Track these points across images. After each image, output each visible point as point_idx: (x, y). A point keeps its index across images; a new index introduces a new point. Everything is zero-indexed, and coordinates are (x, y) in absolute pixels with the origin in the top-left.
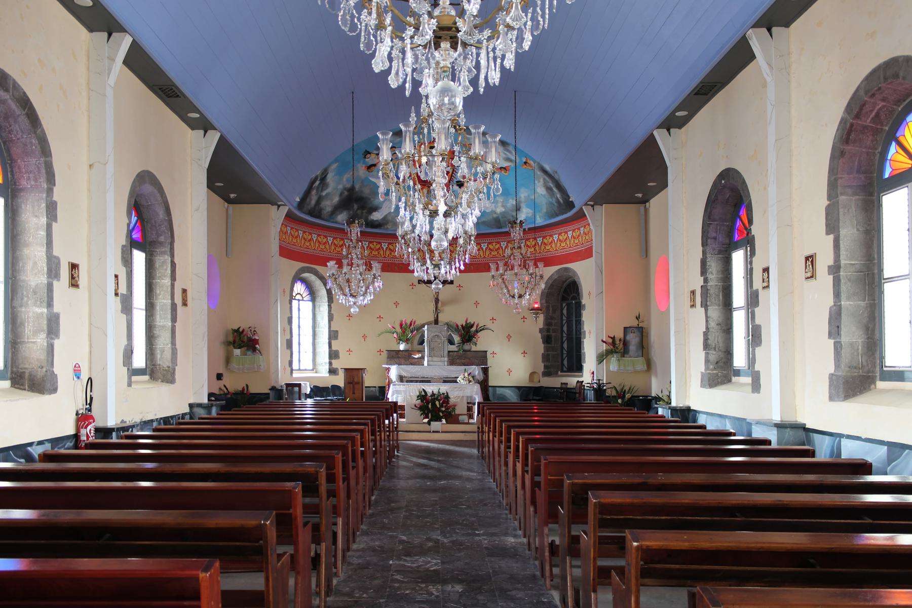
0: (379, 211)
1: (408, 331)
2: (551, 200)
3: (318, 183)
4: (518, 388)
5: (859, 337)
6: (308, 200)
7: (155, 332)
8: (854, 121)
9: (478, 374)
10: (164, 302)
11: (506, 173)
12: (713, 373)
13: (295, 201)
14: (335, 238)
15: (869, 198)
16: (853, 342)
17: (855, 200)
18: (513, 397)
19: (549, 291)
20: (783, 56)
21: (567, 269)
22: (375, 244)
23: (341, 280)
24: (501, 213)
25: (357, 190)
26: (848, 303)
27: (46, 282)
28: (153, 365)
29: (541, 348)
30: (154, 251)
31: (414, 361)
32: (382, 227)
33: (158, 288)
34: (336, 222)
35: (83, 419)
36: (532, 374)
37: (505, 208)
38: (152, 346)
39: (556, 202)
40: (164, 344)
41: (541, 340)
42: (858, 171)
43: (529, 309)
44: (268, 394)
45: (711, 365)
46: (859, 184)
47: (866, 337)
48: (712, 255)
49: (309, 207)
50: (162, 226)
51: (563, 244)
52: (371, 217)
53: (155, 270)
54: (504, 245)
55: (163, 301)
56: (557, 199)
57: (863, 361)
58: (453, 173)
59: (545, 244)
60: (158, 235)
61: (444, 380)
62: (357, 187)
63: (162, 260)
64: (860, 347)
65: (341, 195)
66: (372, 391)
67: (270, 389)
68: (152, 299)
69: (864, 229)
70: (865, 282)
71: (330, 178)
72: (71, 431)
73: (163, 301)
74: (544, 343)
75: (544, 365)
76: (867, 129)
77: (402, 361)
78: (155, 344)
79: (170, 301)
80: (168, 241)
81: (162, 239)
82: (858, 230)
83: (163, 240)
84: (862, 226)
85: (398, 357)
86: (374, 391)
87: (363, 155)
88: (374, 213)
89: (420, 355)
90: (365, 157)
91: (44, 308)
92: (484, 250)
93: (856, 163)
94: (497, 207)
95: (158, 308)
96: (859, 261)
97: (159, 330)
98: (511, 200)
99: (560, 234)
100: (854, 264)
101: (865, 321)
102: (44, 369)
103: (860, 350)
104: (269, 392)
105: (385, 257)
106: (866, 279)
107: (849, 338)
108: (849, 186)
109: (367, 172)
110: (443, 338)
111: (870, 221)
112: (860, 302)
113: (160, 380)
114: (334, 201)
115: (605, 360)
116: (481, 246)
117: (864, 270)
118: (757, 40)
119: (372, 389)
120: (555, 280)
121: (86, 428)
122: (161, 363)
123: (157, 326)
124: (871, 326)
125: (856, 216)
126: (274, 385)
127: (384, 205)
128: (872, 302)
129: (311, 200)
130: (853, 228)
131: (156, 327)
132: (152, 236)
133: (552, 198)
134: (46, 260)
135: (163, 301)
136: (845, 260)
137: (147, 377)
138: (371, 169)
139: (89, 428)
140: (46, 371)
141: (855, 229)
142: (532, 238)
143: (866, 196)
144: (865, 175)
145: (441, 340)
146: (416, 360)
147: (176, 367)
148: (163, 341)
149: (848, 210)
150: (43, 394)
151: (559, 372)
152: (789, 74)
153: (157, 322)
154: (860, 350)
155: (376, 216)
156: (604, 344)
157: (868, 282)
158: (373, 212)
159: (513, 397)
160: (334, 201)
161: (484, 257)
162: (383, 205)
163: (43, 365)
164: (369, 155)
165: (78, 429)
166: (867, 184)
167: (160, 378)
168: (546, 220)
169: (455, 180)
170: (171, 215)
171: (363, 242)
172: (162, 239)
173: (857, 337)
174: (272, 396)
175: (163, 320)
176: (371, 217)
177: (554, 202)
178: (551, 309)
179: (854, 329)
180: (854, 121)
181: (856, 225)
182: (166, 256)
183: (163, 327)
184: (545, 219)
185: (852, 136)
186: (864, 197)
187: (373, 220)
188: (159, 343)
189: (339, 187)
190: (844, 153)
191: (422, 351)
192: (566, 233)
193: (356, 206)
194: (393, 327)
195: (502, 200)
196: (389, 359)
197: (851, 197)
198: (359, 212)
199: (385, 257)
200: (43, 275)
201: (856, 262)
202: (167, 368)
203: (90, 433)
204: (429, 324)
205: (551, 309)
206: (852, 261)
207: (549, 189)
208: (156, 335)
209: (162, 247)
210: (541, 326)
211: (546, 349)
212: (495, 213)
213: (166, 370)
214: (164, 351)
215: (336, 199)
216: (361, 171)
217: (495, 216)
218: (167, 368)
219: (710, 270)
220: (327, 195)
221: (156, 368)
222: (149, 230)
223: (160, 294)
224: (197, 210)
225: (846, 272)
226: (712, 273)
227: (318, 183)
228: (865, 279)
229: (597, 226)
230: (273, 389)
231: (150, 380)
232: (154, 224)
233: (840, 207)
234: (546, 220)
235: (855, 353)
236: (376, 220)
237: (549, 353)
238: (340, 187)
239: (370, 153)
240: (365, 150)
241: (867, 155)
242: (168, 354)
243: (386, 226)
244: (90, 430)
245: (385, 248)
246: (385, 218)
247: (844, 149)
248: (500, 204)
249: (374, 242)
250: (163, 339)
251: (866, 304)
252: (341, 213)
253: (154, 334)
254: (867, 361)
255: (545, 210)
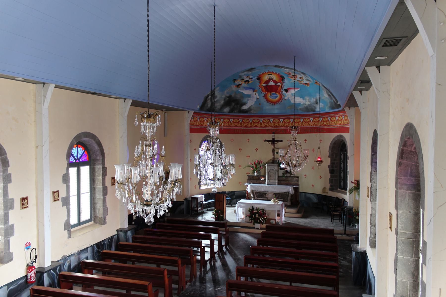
0: (246, 105)
1: (258, 165)
2: (331, 100)
3: (210, 97)
4: (317, 195)
5: (408, 279)
6: (206, 105)
7: (96, 201)
8: (403, 148)
9: (291, 191)
10: (99, 187)
11: (308, 86)
12: (373, 240)
13: (197, 108)
14: (224, 119)
15: (418, 192)
16: (404, 281)
17: (408, 193)
18: (315, 200)
19: (333, 146)
20: (386, 83)
21: (341, 136)
22: (246, 120)
23: (161, 189)
24: (308, 105)
25: (233, 96)
26: (402, 257)
27: (3, 213)
28: (95, 216)
29: (328, 176)
30: (95, 163)
31: (261, 181)
32: (249, 113)
33: (97, 180)
34: (223, 112)
35: (30, 268)
36: (324, 189)
37: (310, 102)
38: (95, 207)
39: (334, 102)
40: (100, 207)
41: (329, 172)
42: (411, 176)
43: (315, 161)
44: (183, 202)
45: (372, 235)
46: (411, 184)
47: (412, 280)
48: (375, 172)
49: (207, 108)
50: (98, 152)
51: (340, 122)
52: (242, 108)
53: (95, 173)
54: (312, 120)
55: (99, 187)
56: (334, 100)
57: (411, 294)
58: (282, 85)
59: (332, 121)
60: (96, 156)
61: (274, 193)
62: (233, 95)
63: (99, 168)
64: (408, 285)
65: (225, 100)
66: (244, 193)
67: (184, 200)
68: (94, 186)
69: (414, 212)
70: (414, 246)
71: (217, 93)
72: (24, 274)
73: (99, 187)
74: (330, 173)
75: (330, 185)
76: (413, 153)
77: (255, 181)
78: (95, 206)
79: (102, 187)
80: (101, 159)
81: (98, 158)
82: (410, 212)
83: (98, 158)
84: (413, 210)
85: (253, 179)
86: (245, 193)
87: (233, 81)
88: (243, 106)
89: (264, 179)
90: (234, 82)
91: (2, 225)
92: (302, 122)
93: (409, 171)
94: (306, 101)
95: (97, 190)
96: (409, 232)
97: (98, 200)
98: (313, 99)
99: (339, 116)
100: (407, 233)
101: (412, 270)
102: (3, 253)
103: (408, 287)
104: (184, 201)
105: (251, 126)
106: (414, 243)
107: (401, 279)
108: (405, 184)
109: (237, 88)
110: (275, 171)
111: (418, 208)
112: (409, 258)
113: (98, 223)
114: (221, 103)
115: (353, 192)
116: (300, 120)
117: (412, 238)
118: (372, 72)
119: (243, 192)
120: (336, 141)
121: (30, 273)
122: (98, 215)
123: (96, 198)
124: (416, 274)
125: (409, 203)
126: (187, 197)
127: (248, 102)
128: (417, 259)
129: (208, 105)
130: (407, 211)
131: (96, 199)
132: (93, 157)
133: (331, 100)
134: (3, 203)
135: (99, 186)
136: (401, 230)
137: (92, 222)
138: (239, 86)
139: (31, 273)
140: (4, 254)
141: (408, 211)
142: (326, 117)
143: (416, 191)
144: (415, 178)
145: (274, 171)
146: (262, 181)
147: (107, 216)
148: (99, 206)
149: (404, 199)
150: (3, 264)
151: (338, 189)
152: (389, 95)
153: (96, 196)
154: (408, 287)
155: (245, 107)
156: (353, 184)
157: (415, 246)
158: (243, 106)
159: (315, 200)
160: (221, 103)
161: (302, 126)
162: (247, 102)
163: (3, 251)
164: (236, 81)
165: (27, 273)
166: (416, 184)
167: (98, 222)
168: (330, 110)
169: (283, 89)
170: (102, 146)
171: (240, 119)
172: (98, 158)
173: (407, 279)
174: (185, 203)
175: (99, 196)
176: (242, 108)
177: (332, 101)
178: (334, 155)
179: (405, 273)
180: (403, 148)
181: (409, 209)
182: (100, 166)
183: (99, 199)
184: (330, 109)
185: (405, 155)
186: (415, 192)
187: (243, 110)
188: (97, 206)
189: (223, 97)
190: (400, 164)
191: (264, 176)
192: (342, 116)
193: (233, 104)
194: (251, 164)
195: (308, 99)
196: (248, 180)
197: (406, 191)
198: (236, 106)
199: (251, 126)
200: (2, 210)
201: (408, 232)
202: (101, 218)
203: (32, 275)
204: (268, 163)
205: (334, 155)
206: (405, 231)
207: (329, 95)
208: (96, 203)
209: (98, 162)
210: (329, 164)
211: (331, 176)
212: (306, 105)
213: (100, 219)
214: (99, 210)
215: (222, 102)
216: (234, 88)
217: (305, 106)
218: (101, 218)
219: (374, 181)
220: (217, 101)
221: (96, 218)
222: (92, 154)
223: (98, 183)
224: (122, 137)
225: (401, 237)
226: (374, 182)
227: (210, 97)
228: (413, 244)
229: (351, 119)
230: (186, 199)
231: (94, 223)
232: (94, 151)
233: (399, 196)
234: (330, 110)
235: (405, 288)
236: (245, 109)
237: (333, 178)
238: (224, 96)
239: (237, 80)
240: (233, 79)
241: (416, 166)
242: (101, 211)
243: (250, 112)
244: (32, 274)
245: (251, 122)
246: (249, 108)
247: (400, 161)
248: (307, 100)
249: (245, 119)
250: (99, 204)
251: (413, 259)
252: (226, 108)
253: (95, 202)
254: (412, 295)
255: (329, 105)
